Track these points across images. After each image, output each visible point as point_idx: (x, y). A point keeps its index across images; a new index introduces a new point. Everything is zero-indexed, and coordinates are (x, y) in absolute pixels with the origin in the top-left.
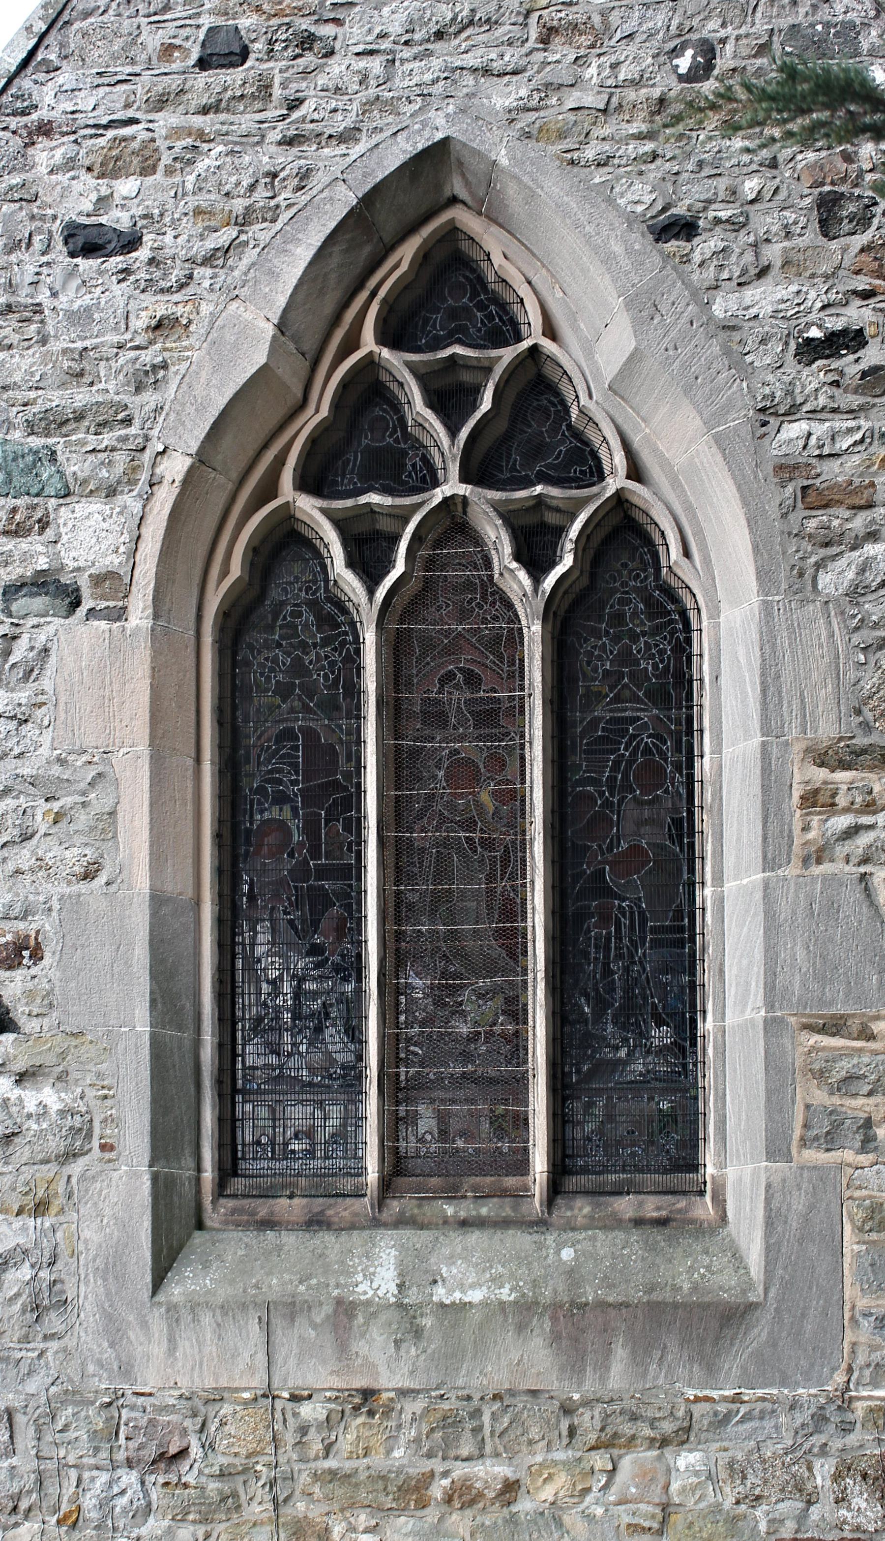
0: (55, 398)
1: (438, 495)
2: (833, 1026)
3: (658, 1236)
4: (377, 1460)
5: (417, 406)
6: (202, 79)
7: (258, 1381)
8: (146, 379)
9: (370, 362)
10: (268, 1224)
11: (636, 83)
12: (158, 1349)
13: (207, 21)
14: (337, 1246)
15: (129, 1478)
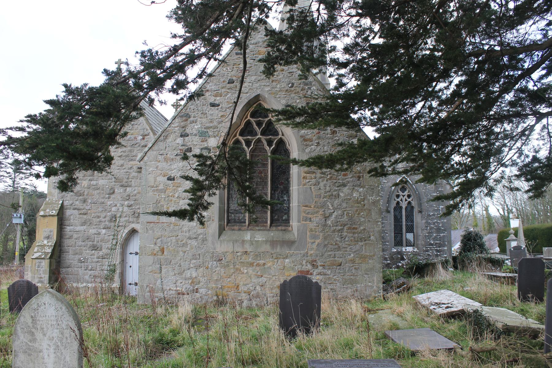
0: (208, 125)
1: (257, 137)
2: (306, 206)
3: (284, 232)
4: (247, 260)
5: (255, 126)
6: (228, 85)
7: (232, 250)
8: (220, 123)
9: (249, 120)
10: (233, 230)
11: (284, 88)
12: (219, 246)
13: (229, 78)
14: (113, 183)
15: (215, 263)
